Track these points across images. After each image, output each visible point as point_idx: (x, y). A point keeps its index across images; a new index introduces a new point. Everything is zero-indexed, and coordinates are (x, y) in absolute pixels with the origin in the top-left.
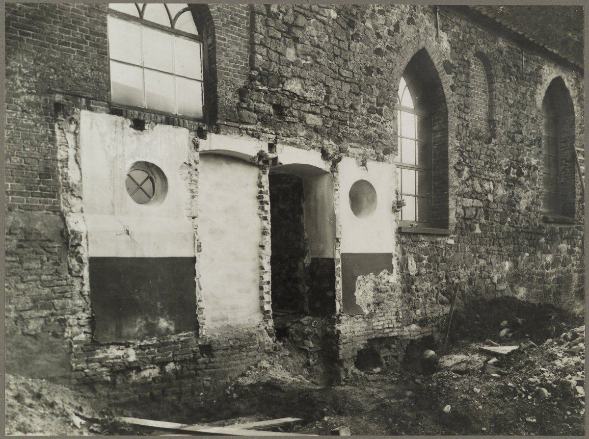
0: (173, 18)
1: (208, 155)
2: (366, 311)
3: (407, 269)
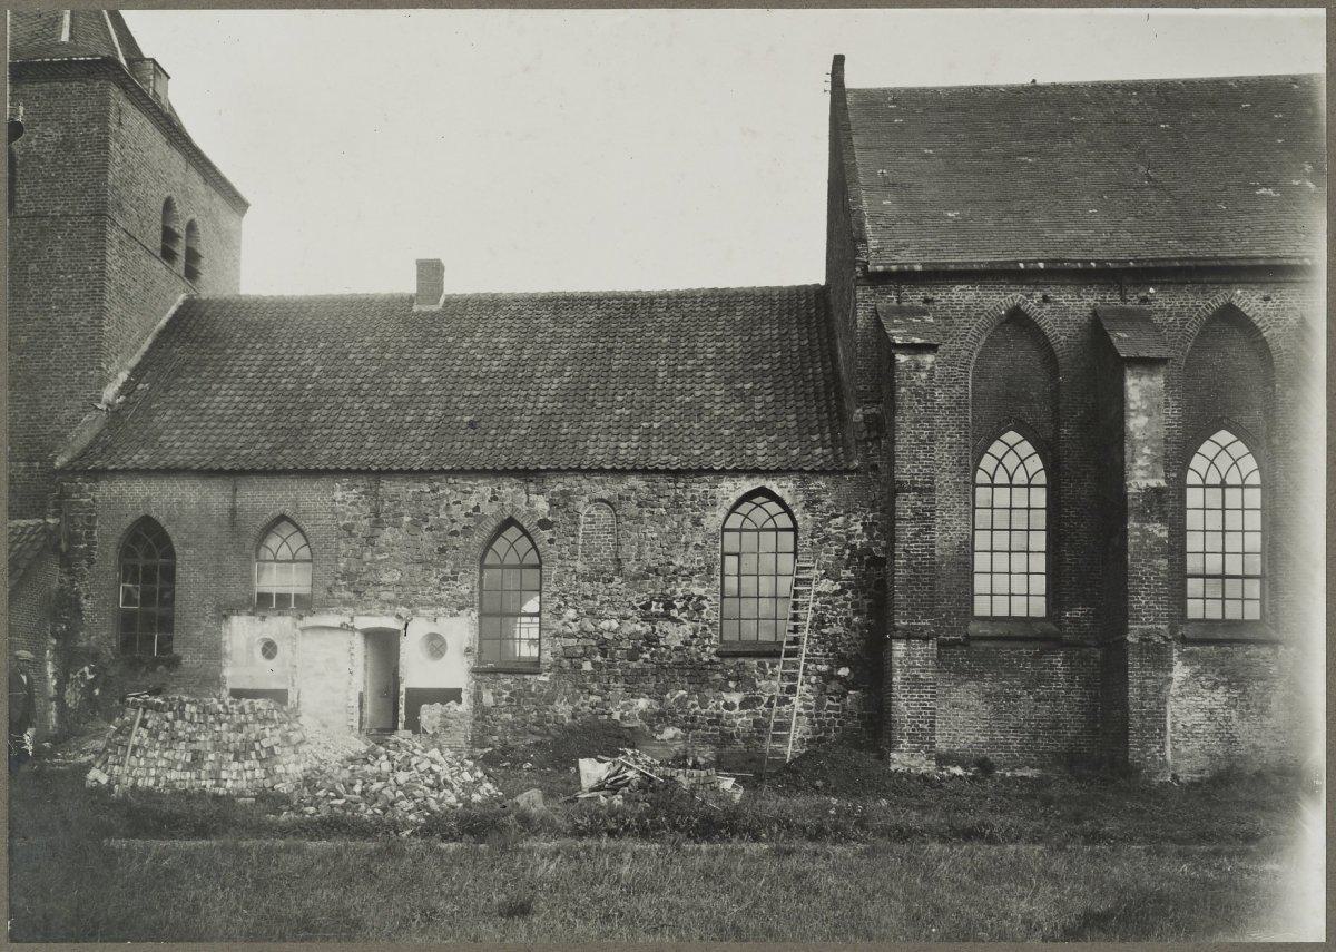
0: (1011, 474)
1: (303, 630)
2: (431, 732)
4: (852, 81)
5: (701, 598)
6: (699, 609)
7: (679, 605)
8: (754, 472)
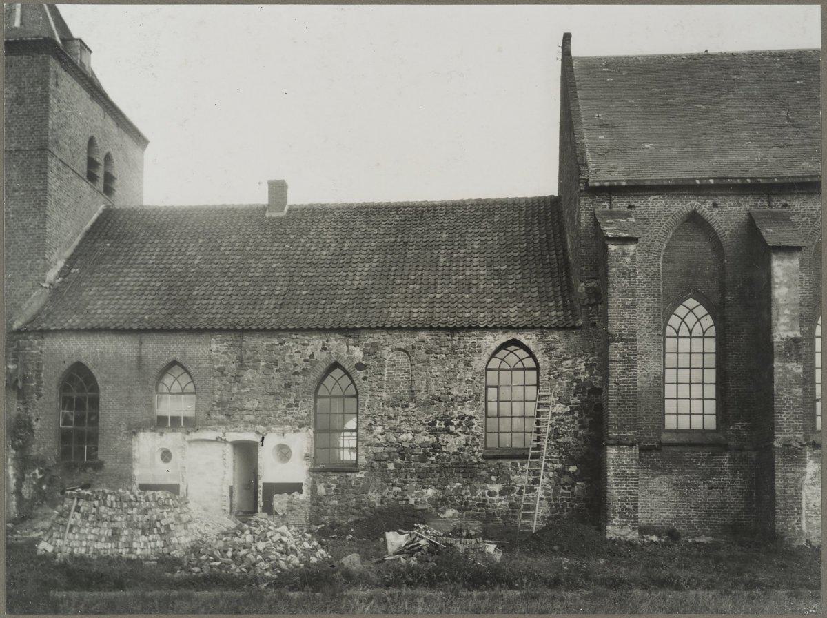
1: (190, 442)
2: (281, 514)
3: (316, 492)
4: (577, 51)
5: (471, 417)
6: (470, 425)
7: (456, 423)
8: (509, 328)
